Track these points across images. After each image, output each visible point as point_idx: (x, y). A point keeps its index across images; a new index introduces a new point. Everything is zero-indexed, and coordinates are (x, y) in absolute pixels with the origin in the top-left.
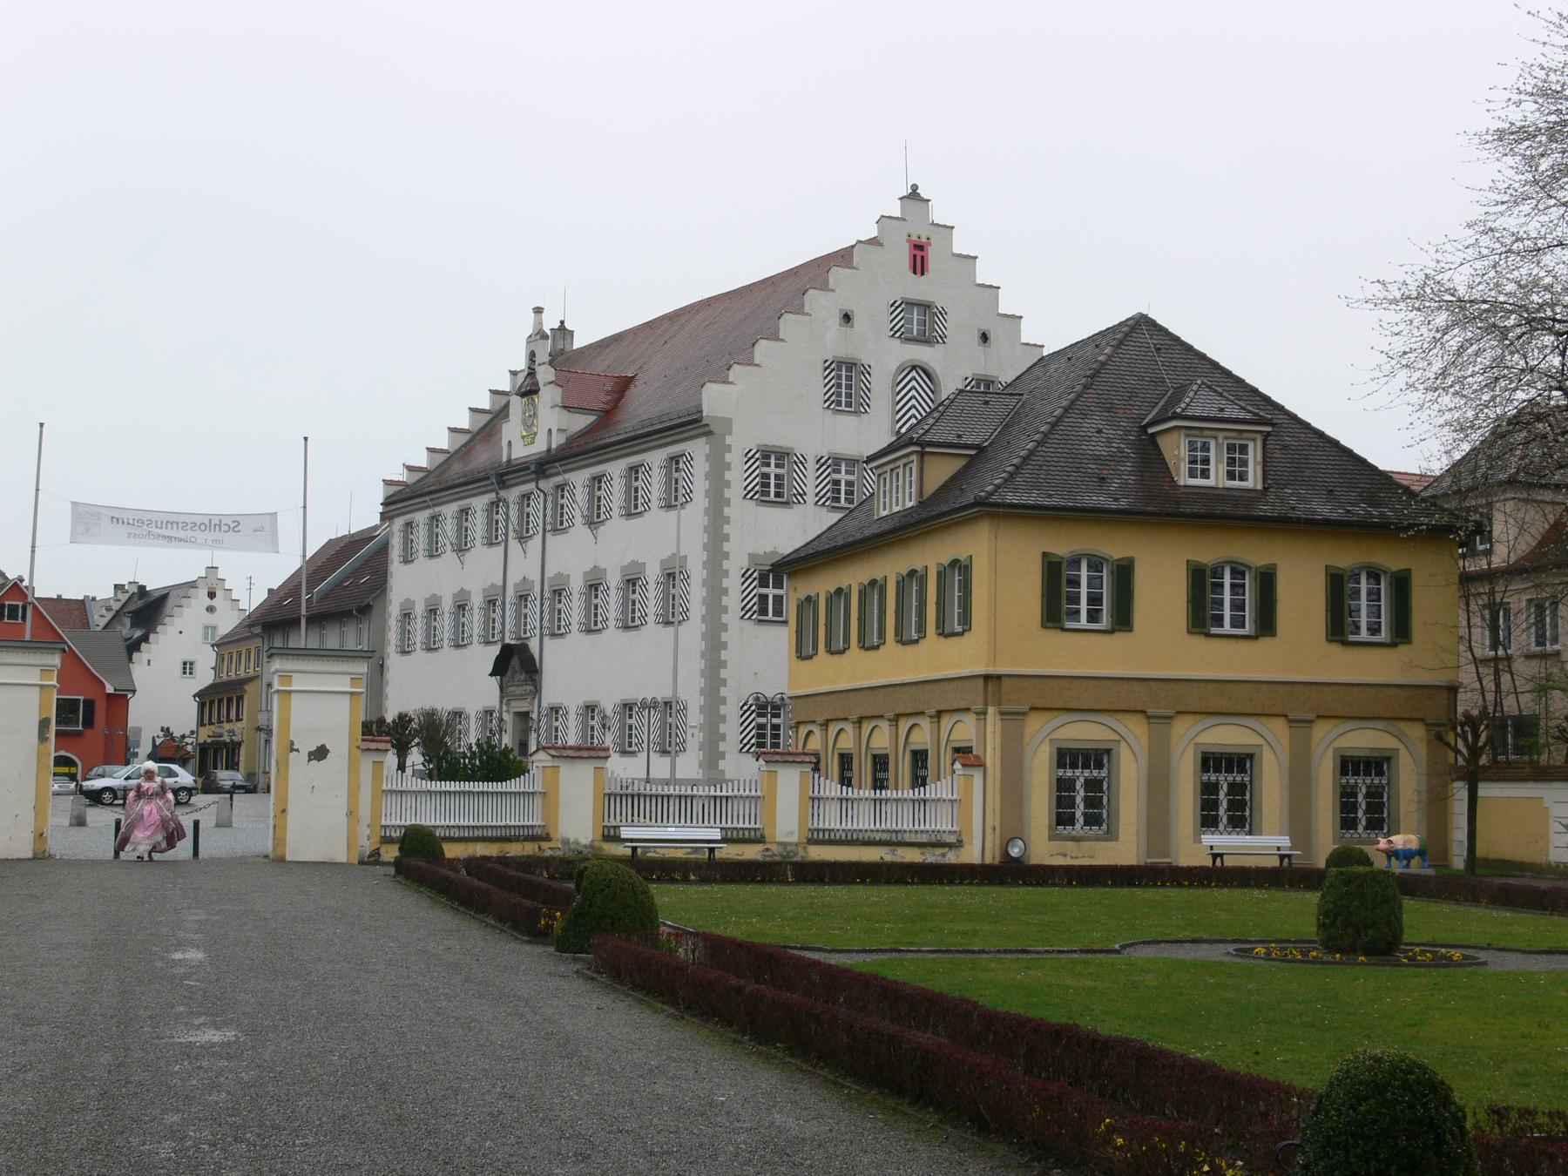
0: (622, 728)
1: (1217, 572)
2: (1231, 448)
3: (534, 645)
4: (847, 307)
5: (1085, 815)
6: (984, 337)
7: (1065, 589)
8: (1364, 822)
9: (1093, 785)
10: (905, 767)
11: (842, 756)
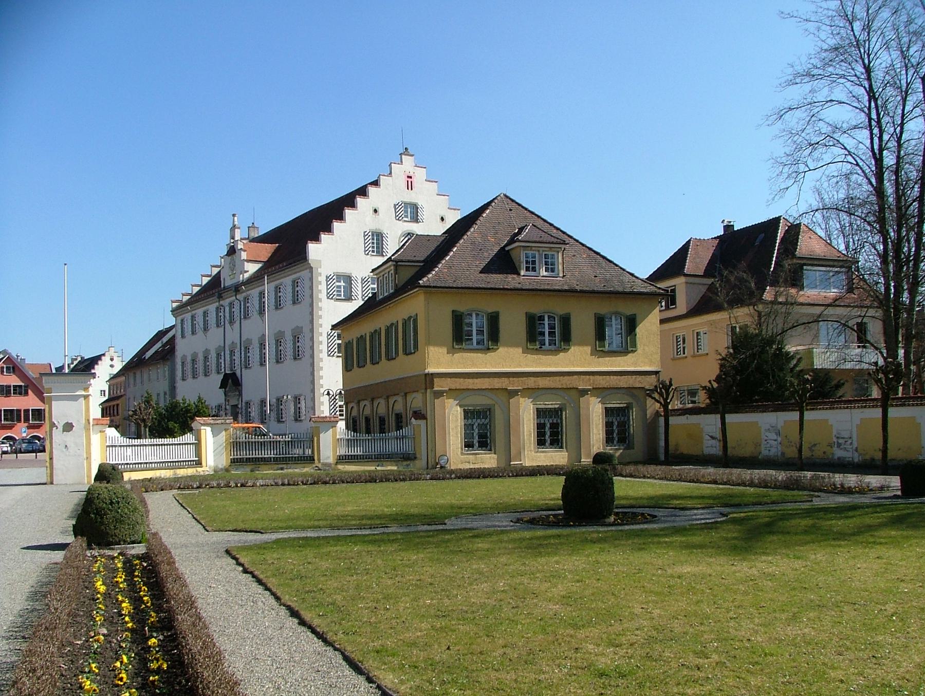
0: (278, 410)
1: (541, 318)
2: (546, 256)
3: (238, 373)
4: (376, 207)
5: (479, 442)
6: (375, 211)
7: (466, 328)
8: (549, 441)
9: (553, 426)
10: (392, 421)
11: (366, 418)
